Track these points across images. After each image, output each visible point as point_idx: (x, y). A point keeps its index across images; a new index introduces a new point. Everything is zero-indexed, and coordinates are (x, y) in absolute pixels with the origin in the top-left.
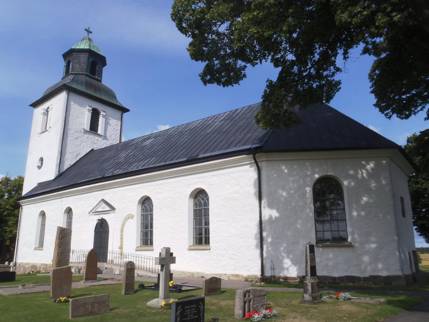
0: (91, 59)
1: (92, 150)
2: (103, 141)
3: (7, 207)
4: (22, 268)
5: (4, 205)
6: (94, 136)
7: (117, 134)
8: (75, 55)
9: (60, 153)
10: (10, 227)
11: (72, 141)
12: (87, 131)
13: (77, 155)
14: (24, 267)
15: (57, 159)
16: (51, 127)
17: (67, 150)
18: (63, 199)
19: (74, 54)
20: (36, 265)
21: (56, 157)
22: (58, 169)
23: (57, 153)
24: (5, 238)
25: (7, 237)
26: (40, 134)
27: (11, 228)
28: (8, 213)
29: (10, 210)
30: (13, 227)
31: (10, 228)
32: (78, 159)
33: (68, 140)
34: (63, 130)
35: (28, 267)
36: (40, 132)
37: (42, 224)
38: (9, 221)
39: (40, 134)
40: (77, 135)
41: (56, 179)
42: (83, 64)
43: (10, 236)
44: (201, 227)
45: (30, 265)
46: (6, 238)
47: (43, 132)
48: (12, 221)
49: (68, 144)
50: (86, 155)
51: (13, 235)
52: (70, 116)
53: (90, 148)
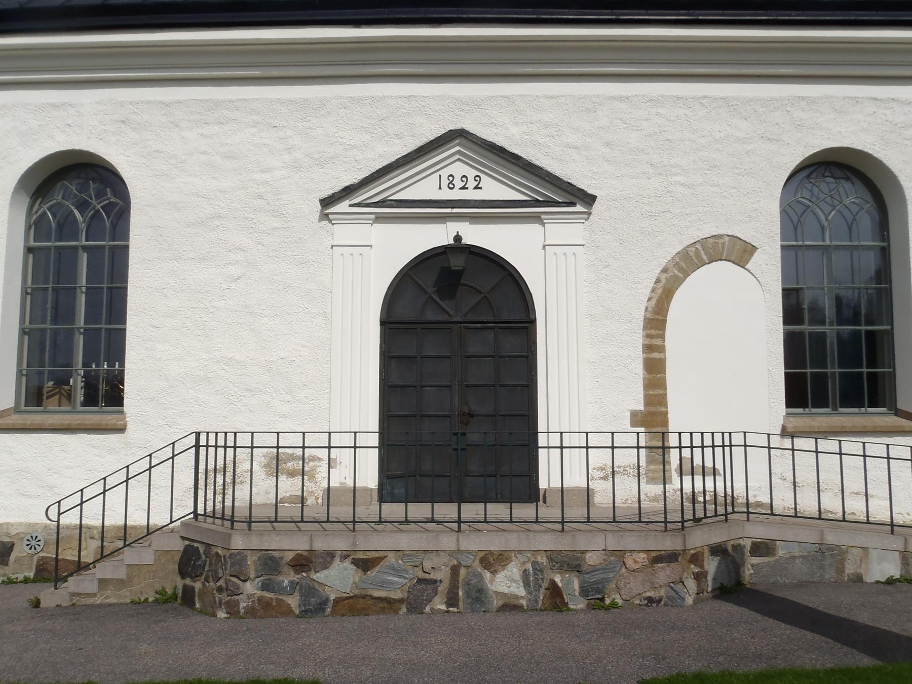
44: (74, 326)
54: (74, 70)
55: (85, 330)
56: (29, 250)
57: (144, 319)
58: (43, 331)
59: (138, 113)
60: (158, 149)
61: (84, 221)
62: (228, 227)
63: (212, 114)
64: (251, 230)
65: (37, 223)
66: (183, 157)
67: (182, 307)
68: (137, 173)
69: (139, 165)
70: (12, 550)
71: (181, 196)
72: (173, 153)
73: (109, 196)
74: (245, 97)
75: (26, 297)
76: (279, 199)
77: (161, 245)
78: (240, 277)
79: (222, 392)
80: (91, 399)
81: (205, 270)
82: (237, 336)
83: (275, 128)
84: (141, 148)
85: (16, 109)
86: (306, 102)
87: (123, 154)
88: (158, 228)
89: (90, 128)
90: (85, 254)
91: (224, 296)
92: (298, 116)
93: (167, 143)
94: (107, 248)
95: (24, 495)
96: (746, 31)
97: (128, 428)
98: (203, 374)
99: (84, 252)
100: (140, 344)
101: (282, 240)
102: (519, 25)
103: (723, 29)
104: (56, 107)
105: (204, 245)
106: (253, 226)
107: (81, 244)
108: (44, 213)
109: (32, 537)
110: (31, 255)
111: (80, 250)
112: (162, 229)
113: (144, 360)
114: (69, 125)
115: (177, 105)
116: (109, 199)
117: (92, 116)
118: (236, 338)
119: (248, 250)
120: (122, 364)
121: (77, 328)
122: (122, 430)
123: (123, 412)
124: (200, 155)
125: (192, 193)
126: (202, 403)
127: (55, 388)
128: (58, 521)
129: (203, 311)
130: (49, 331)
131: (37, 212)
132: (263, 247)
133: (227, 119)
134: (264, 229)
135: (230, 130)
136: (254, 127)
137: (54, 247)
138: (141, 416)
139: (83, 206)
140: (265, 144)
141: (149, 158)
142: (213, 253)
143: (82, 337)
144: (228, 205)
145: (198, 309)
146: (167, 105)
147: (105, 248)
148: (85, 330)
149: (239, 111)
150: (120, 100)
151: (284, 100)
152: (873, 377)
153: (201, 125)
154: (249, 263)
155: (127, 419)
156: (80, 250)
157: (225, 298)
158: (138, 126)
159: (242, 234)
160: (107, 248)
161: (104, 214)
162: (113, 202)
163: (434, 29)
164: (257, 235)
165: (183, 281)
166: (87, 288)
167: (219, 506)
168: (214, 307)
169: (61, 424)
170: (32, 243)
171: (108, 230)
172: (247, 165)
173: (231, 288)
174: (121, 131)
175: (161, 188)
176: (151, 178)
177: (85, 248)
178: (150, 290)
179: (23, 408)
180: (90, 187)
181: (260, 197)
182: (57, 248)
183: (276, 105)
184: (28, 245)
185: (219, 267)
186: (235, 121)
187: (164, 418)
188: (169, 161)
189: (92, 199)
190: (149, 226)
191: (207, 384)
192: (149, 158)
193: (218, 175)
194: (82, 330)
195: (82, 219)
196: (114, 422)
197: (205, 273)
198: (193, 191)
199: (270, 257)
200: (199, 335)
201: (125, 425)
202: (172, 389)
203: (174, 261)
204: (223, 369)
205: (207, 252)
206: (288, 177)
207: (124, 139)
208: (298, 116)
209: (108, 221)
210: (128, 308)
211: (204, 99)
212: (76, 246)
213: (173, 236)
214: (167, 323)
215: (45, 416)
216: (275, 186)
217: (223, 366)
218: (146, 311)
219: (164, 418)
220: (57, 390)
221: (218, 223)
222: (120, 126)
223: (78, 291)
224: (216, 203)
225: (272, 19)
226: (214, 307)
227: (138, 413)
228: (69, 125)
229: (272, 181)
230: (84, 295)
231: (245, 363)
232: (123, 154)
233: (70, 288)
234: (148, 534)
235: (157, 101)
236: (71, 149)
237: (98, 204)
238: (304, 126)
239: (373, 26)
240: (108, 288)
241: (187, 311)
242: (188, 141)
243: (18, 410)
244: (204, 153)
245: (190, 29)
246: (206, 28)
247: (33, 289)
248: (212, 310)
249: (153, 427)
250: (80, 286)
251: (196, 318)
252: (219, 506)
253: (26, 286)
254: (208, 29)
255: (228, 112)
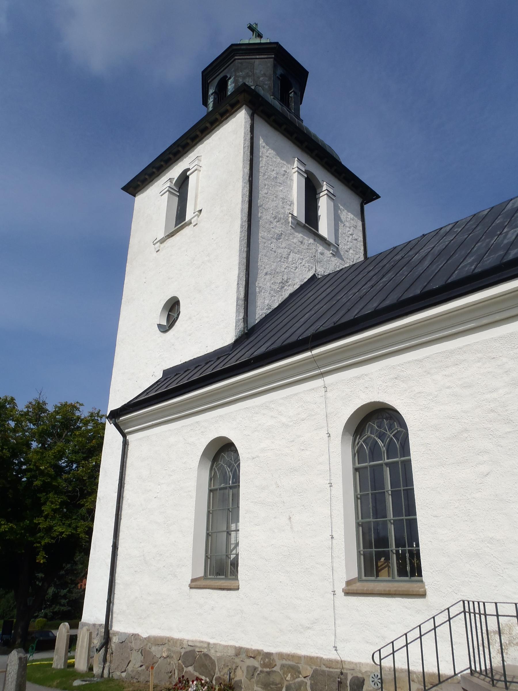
0: (280, 71)
1: (314, 278)
2: (333, 259)
3: (42, 468)
4: (136, 659)
5: (35, 463)
6: (315, 240)
7: (358, 250)
8: (239, 61)
9: (244, 267)
10: (46, 517)
11: (270, 242)
12: (299, 223)
13: (284, 284)
14: (143, 652)
15: (238, 284)
16: (200, 211)
17: (259, 264)
18: (329, 379)
19: (236, 57)
20: (205, 651)
21: (235, 278)
22: (242, 316)
23: (238, 267)
24: (35, 545)
25: (38, 545)
26: (162, 241)
27: (48, 520)
28: (44, 481)
29: (50, 476)
30: (53, 518)
31: (46, 521)
32: (286, 295)
33: (260, 235)
34: (247, 206)
35: (165, 655)
36: (161, 235)
37: (210, 491)
38: (45, 503)
39: (162, 241)
40: (279, 228)
41: (238, 342)
42: (261, 79)
43: (47, 540)
44: (386, 519)
45: (178, 649)
46: (37, 547)
47: (171, 235)
48: (52, 503)
49: (261, 246)
50: (302, 287)
51: (53, 538)
52: (261, 174)
53: (309, 270)
54: (198, 406)
55: (394, 520)
56: (356, 470)
57: (427, 511)
58: (370, 522)
59: (404, 371)
60: (420, 391)
61: (385, 446)
62: (474, 437)
63: (450, 360)
64: (491, 437)
65: (358, 452)
66: (436, 393)
67: (451, 500)
68: (409, 410)
69: (409, 404)
70: (364, 684)
71: (439, 420)
72: (429, 392)
73: (396, 427)
74: (469, 343)
75: (357, 501)
76: (507, 410)
77: (431, 456)
78: (489, 473)
79: (490, 565)
80: (402, 572)
81: (463, 470)
82: (494, 520)
83: (494, 359)
84: (409, 392)
85: (338, 384)
86: (512, 336)
87: (399, 399)
88: (427, 445)
89: (378, 387)
90: (388, 468)
91: (479, 489)
92: (508, 346)
93: (424, 386)
94: (400, 462)
95: (368, 642)
96: (259, 370)
97: (427, 594)
98: (474, 551)
99: (387, 467)
100: (427, 530)
101: (515, 441)
102: (418, 312)
103: (424, 312)
104: (358, 378)
105: (460, 453)
106: (491, 433)
107: (384, 462)
108: (362, 445)
109: (375, 675)
110: (358, 473)
111: (384, 466)
112: (430, 445)
113: (432, 542)
114: (366, 387)
115: (426, 359)
116: (397, 429)
117: (378, 379)
118: (493, 521)
119: (491, 452)
120: (418, 545)
121: (389, 520)
122: (423, 595)
123: (423, 581)
124: (447, 390)
125: (445, 416)
126: (477, 575)
127: (385, 563)
128: (380, 665)
129: (466, 501)
130: (372, 522)
131: (358, 444)
132: (501, 448)
133: (460, 361)
134: (500, 435)
135: (463, 368)
136: (479, 361)
137: (369, 466)
138: (435, 585)
139: (381, 436)
140: (489, 372)
141: (415, 398)
142: (466, 457)
143: (392, 526)
144: (471, 421)
145: (462, 501)
146: (420, 361)
147: (398, 463)
148: (394, 520)
149: (467, 353)
150: (392, 365)
151: (496, 338)
152: (410, 552)
153: (444, 369)
154: (494, 462)
155: (426, 587)
156: (384, 466)
157: (481, 490)
158: (405, 379)
159: (484, 440)
160: (400, 462)
161: (395, 440)
162: (399, 431)
163: (362, 334)
164: (495, 439)
165: (449, 481)
166: (392, 491)
167: (483, 668)
168: (474, 498)
169: (384, 590)
170: (357, 465)
171: (399, 450)
172: (479, 389)
173: (484, 482)
174: (396, 384)
175: (425, 417)
176: (418, 411)
177: (387, 464)
178: (428, 490)
179: (364, 578)
180: (384, 423)
181: (492, 411)
182: (371, 466)
183: (491, 343)
184: (355, 467)
185: (472, 467)
186: (465, 361)
187: (451, 586)
188: (428, 398)
189: (387, 432)
190: (422, 445)
191: (478, 559)
192: (415, 398)
193: (460, 401)
194: (392, 521)
195: (383, 445)
196: (417, 589)
197: (463, 473)
198: (446, 415)
199: (508, 455)
200: (466, 521)
201: (425, 591)
202: (453, 564)
203: (441, 467)
204: (488, 547)
205: (462, 458)
206: (511, 392)
207: (398, 389)
208: (508, 346)
209: (367, 449)
210: (416, 504)
211: (442, 352)
212: (381, 463)
213: (438, 449)
214: (443, 513)
215: (376, 584)
216: (501, 401)
217: (488, 545)
218: (428, 505)
219: (451, 586)
220: (386, 564)
221: (466, 435)
222: (395, 382)
223: (386, 494)
224: (463, 421)
225: (480, 285)
226: (474, 498)
227: (433, 583)
228: (366, 387)
229: (498, 397)
230: (390, 496)
231: (503, 541)
232: (399, 399)
233: (381, 493)
234: (440, 682)
235: (414, 360)
236: (369, 402)
237: (391, 434)
238: (514, 353)
239: (414, 313)
240: (403, 490)
241: (455, 502)
242: (437, 381)
243: (360, 579)
244: (448, 387)
245: (368, 330)
246: (434, 307)
247: (361, 496)
248: (472, 500)
249: (444, 593)
250: (387, 491)
251: (462, 507)
252: (483, 668)
253: (357, 494)
254: (435, 307)
255: (460, 356)
